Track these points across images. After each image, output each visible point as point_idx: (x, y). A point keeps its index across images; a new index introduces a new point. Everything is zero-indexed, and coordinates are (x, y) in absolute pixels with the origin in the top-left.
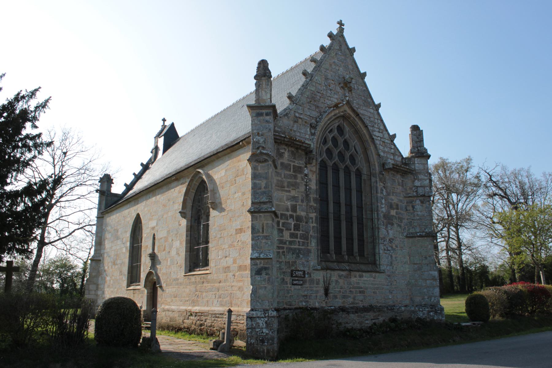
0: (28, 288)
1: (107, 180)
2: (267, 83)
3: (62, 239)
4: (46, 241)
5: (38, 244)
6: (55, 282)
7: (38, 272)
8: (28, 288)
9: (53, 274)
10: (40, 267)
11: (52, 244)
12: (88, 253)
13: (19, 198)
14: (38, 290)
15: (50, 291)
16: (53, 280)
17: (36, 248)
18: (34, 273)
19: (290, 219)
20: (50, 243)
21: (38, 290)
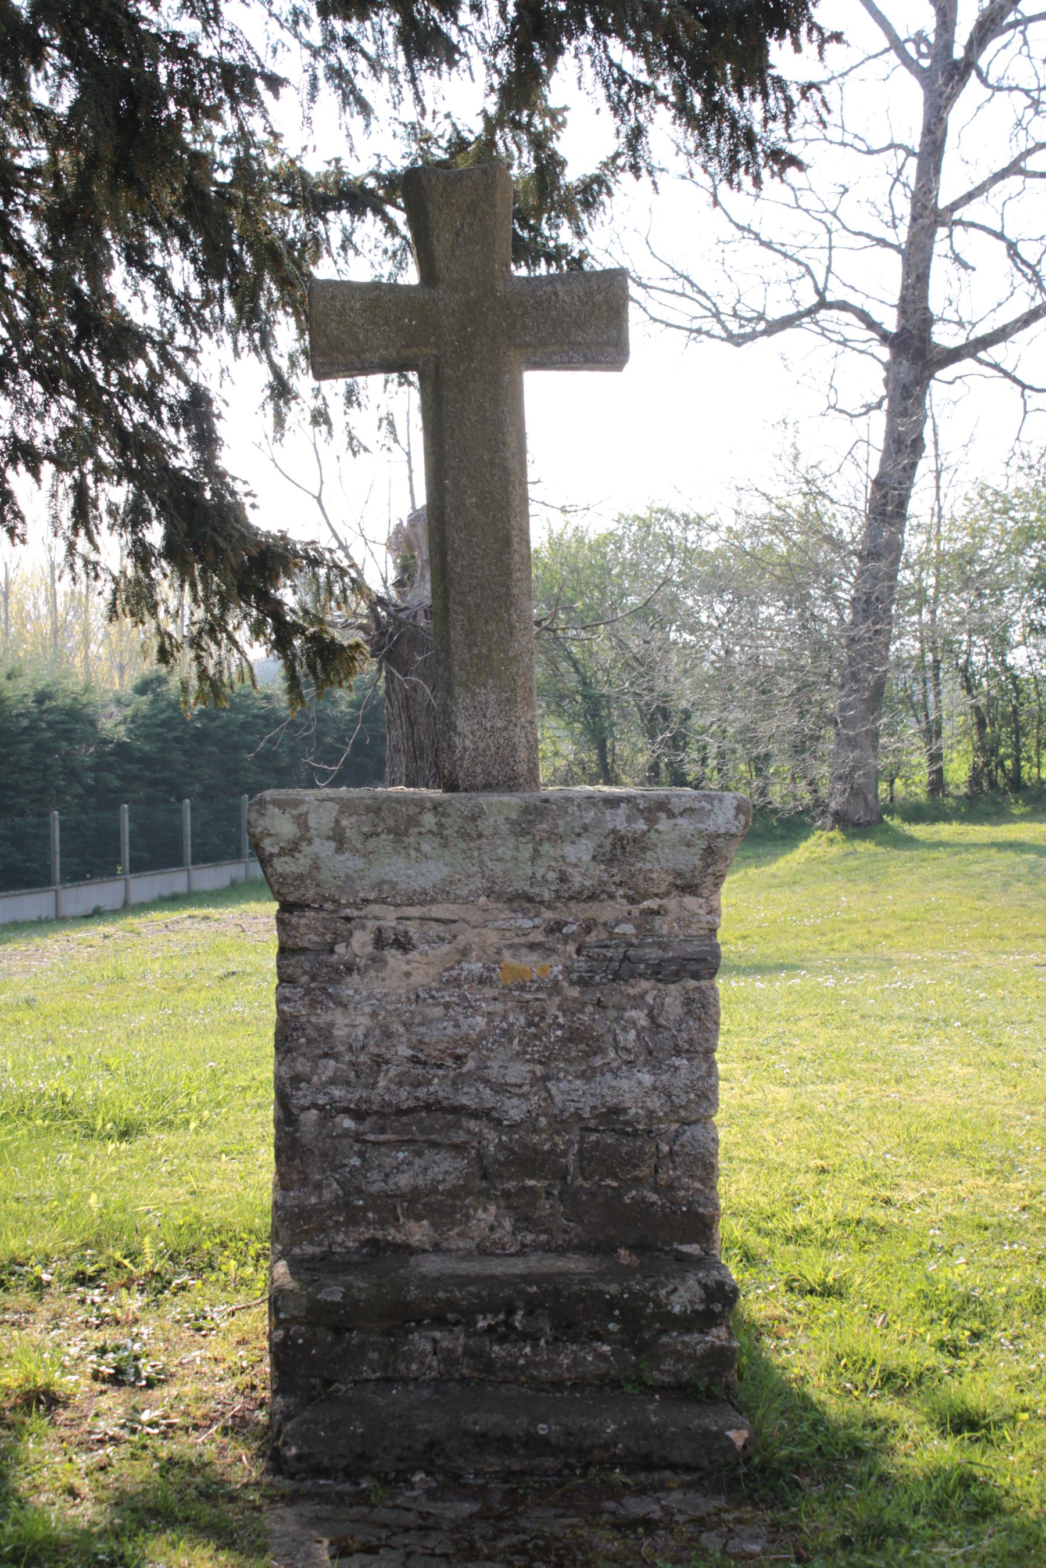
0: (854, 677)
1: (357, 253)
2: (93, 574)
3: (999, 230)
4: (944, 336)
5: (887, 367)
6: (1016, 634)
7: (905, 577)
8: (854, 677)
9: (998, 588)
10: (913, 542)
11: (981, 355)
12: (892, 57)
13: (87, 30)
14: (917, 688)
15: (993, 692)
16: (1006, 624)
17: (879, 406)
18: (882, 565)
19: (569, 43)
20: (973, 348)
21: (917, 688)
